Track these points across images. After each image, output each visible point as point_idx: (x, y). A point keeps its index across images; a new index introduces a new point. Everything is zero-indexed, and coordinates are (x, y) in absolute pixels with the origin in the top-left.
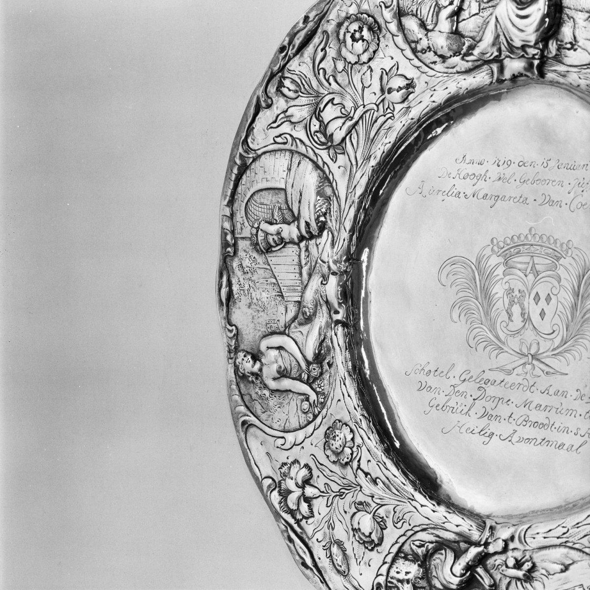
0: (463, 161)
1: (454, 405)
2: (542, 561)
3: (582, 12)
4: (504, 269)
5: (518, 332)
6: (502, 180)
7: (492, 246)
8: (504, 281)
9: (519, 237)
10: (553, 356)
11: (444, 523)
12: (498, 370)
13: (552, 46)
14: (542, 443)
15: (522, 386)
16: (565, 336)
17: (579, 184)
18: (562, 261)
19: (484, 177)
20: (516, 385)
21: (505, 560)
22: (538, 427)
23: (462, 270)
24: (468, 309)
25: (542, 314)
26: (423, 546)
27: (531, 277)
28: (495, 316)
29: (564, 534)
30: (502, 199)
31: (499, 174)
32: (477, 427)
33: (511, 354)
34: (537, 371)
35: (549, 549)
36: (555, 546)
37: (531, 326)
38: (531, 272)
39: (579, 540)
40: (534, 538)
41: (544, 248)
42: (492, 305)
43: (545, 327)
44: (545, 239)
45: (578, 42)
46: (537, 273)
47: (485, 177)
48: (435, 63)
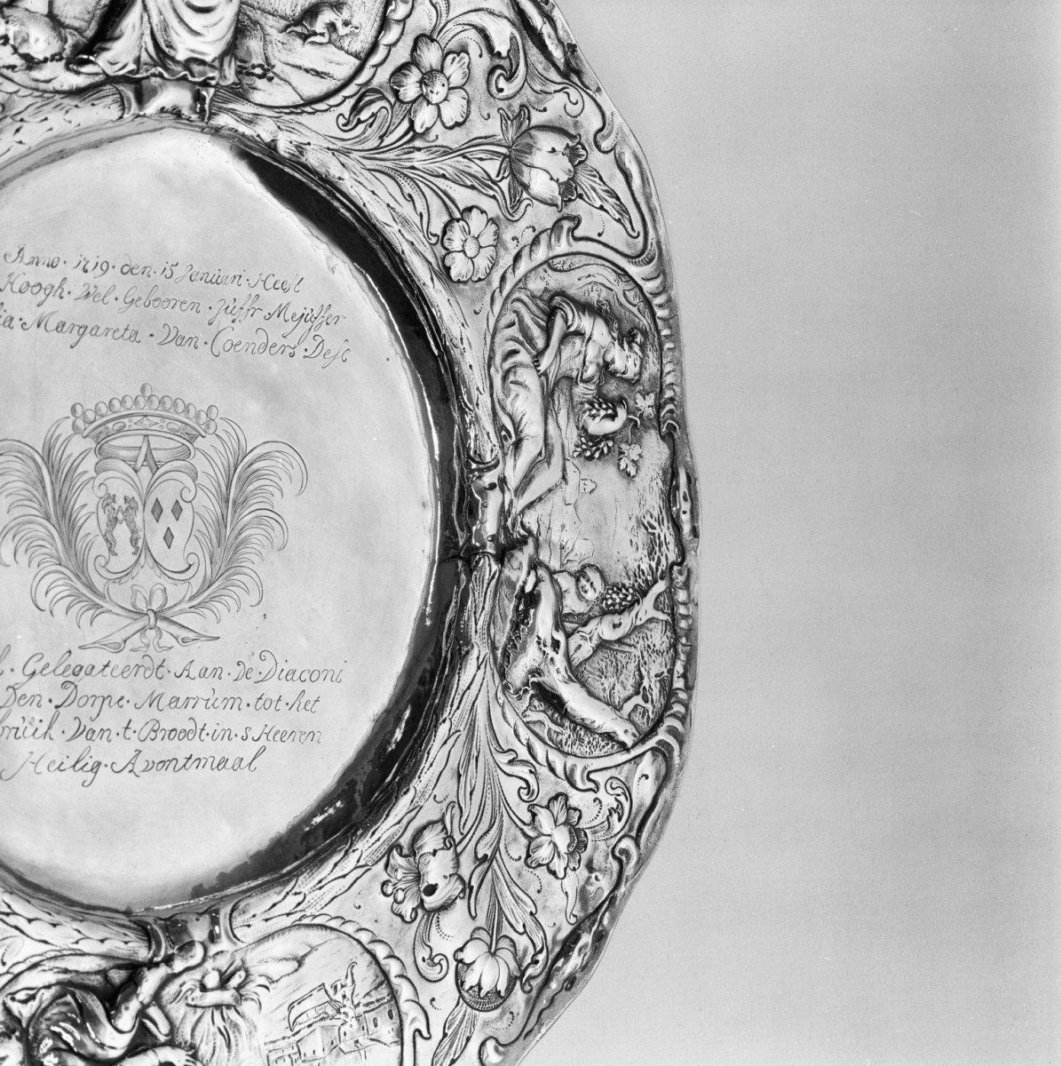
0: (19, 259)
1: (18, 723)
2: (260, 962)
3: (273, 15)
4: (97, 460)
5: (127, 573)
6: (91, 298)
7: (72, 418)
8: (97, 482)
9: (122, 402)
10: (193, 609)
11: (77, 943)
12: (97, 645)
13: (229, 66)
14: (187, 767)
15: (142, 669)
16: (209, 572)
17: (227, 308)
18: (199, 442)
19: (59, 291)
20: (132, 667)
21: (199, 978)
22: (176, 738)
23: (18, 466)
24: (31, 538)
25: (168, 537)
26: (32, 997)
27: (145, 473)
28: (84, 546)
29: (299, 904)
30: (93, 332)
31: (86, 286)
32: (68, 757)
33: (117, 614)
34: (167, 640)
35: (273, 938)
36: (282, 931)
37: (150, 561)
38: (145, 463)
39: (322, 908)
40: (249, 926)
41: (168, 421)
42: (77, 528)
43: (173, 559)
44: (168, 404)
45: (273, 67)
46: (155, 466)
47: (60, 290)
48: (12, 67)
